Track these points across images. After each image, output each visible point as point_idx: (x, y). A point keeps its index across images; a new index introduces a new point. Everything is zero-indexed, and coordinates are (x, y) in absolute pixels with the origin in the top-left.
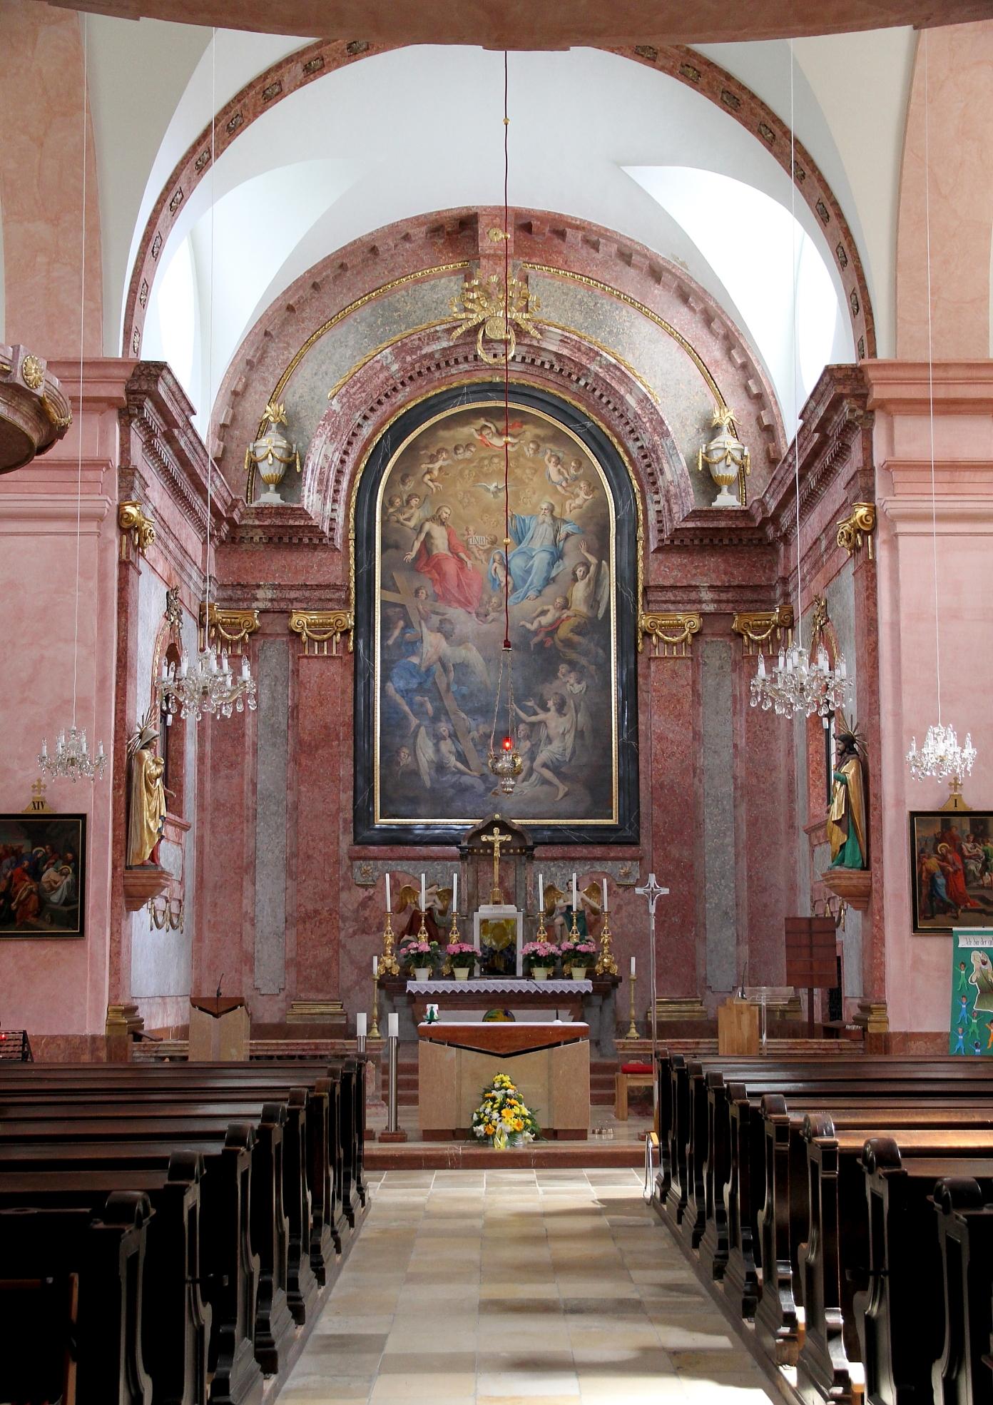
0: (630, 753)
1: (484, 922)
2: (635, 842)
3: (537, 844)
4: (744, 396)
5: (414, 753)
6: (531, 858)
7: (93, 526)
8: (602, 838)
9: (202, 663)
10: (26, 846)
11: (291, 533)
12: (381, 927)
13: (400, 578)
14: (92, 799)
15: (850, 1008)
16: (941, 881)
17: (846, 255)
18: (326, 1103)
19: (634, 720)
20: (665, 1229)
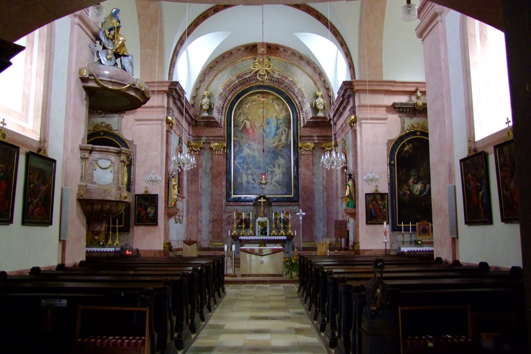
0: (297, 178)
1: (259, 222)
2: (298, 201)
3: (273, 202)
4: (324, 88)
5: (241, 179)
6: (271, 205)
7: (160, 122)
8: (289, 200)
9: (185, 156)
10: (143, 202)
11: (211, 123)
12: (233, 223)
13: (238, 134)
14: (159, 190)
15: (351, 243)
16: (373, 211)
17: (348, 55)
18: (212, 267)
19: (297, 170)
20: (299, 299)
